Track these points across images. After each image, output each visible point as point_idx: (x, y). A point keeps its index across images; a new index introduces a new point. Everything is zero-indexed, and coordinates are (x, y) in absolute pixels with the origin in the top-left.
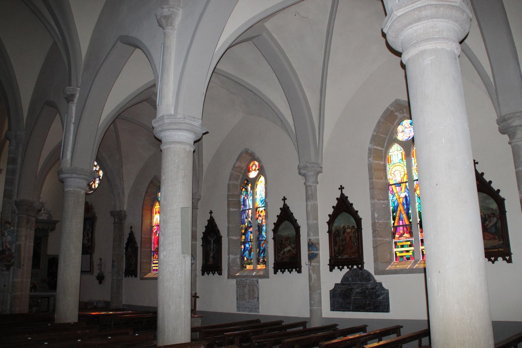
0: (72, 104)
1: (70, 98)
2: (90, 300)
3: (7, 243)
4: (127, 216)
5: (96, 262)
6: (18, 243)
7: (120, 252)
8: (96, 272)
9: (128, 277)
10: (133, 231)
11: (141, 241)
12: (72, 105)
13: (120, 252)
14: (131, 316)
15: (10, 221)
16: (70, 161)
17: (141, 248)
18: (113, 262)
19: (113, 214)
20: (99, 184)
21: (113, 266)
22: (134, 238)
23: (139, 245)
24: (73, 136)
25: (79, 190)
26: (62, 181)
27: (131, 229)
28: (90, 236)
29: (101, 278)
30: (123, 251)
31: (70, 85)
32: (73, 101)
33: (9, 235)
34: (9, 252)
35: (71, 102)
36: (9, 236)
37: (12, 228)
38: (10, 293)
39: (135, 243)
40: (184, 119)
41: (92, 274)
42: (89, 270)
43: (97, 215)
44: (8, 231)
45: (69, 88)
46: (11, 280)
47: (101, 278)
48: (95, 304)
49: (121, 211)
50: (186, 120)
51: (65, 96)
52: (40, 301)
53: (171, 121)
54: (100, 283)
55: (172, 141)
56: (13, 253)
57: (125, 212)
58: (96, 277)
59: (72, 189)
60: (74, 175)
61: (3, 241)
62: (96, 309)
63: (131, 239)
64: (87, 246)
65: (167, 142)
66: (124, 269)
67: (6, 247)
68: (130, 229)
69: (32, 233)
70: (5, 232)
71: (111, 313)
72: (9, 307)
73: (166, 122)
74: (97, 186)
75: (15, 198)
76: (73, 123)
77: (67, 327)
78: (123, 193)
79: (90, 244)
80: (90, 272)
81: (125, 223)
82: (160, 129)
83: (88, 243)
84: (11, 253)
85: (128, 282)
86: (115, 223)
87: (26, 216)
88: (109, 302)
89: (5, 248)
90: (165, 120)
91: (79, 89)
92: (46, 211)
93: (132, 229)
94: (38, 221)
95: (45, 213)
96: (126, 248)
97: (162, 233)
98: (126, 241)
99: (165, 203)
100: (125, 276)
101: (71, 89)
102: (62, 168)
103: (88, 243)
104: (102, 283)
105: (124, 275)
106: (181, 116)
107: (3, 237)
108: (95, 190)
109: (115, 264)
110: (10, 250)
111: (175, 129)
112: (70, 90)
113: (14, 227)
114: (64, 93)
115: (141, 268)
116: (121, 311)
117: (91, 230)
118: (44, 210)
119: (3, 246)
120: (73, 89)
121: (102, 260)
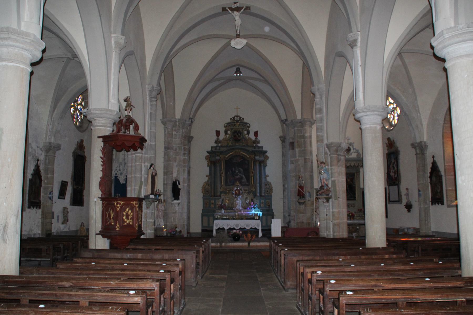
0: (357, 48)
1: (353, 45)
2: (401, 227)
3: (324, 180)
4: (428, 146)
5: (403, 192)
6: (333, 179)
7: (425, 182)
8: (404, 201)
9: (435, 205)
10: (435, 161)
11: (445, 170)
12: (356, 49)
13: (425, 182)
14: (439, 243)
15: (324, 161)
16: (363, 101)
17: (445, 176)
18: (419, 191)
19: (413, 146)
20: (398, 120)
21: (419, 195)
22: (437, 167)
23: (443, 173)
24: (362, 78)
25: (375, 126)
26: (358, 121)
27: (433, 159)
28: (396, 168)
29: (409, 207)
30: (428, 181)
31: (351, 32)
32: (356, 45)
33: (325, 173)
34: (327, 187)
35: (355, 47)
36: (325, 174)
37: (327, 167)
38: (332, 221)
39: (439, 171)
40: (468, 27)
41: (401, 203)
42: (397, 200)
43: (399, 149)
44: (324, 170)
45: (351, 34)
46: (331, 210)
47: (409, 207)
48: (406, 231)
49: (421, 142)
50: (471, 28)
51: (349, 43)
52: (358, 228)
53: (451, 34)
54: (409, 211)
55: (457, 56)
56: (330, 188)
57: (425, 142)
58: (404, 205)
59: (368, 126)
60: (368, 113)
61: (321, 178)
62: (406, 235)
63: (435, 167)
64: (394, 178)
65: (451, 59)
66: (430, 198)
67: (324, 182)
68: (432, 159)
69: (343, 170)
70: (321, 170)
71: (420, 239)
72: (332, 233)
73: (447, 37)
74: (396, 121)
75: (325, 142)
76: (361, 66)
77: (375, 251)
78: (422, 125)
79: (396, 176)
80: (398, 201)
81: (426, 153)
82: (440, 46)
83: (395, 175)
84: (329, 188)
85: (435, 209)
86: (416, 154)
87: (336, 156)
88: (418, 229)
89: (323, 184)
90: (444, 35)
91: (359, 33)
92: (355, 151)
93: (435, 159)
94: (347, 160)
95: (355, 152)
96: (431, 177)
97: (458, 157)
98: (429, 170)
99: (458, 124)
100: (432, 205)
101: (352, 35)
102: (357, 108)
103: (395, 175)
104: (411, 211)
105: (431, 203)
106: (463, 25)
107: (321, 175)
108: (396, 125)
109: (421, 193)
110: (327, 185)
111: (458, 43)
112: (352, 36)
113: (328, 166)
114: (347, 40)
115: (447, 196)
116: (429, 238)
117: (396, 163)
118: (353, 150)
119: (321, 183)
120: (354, 34)
121: (409, 190)
